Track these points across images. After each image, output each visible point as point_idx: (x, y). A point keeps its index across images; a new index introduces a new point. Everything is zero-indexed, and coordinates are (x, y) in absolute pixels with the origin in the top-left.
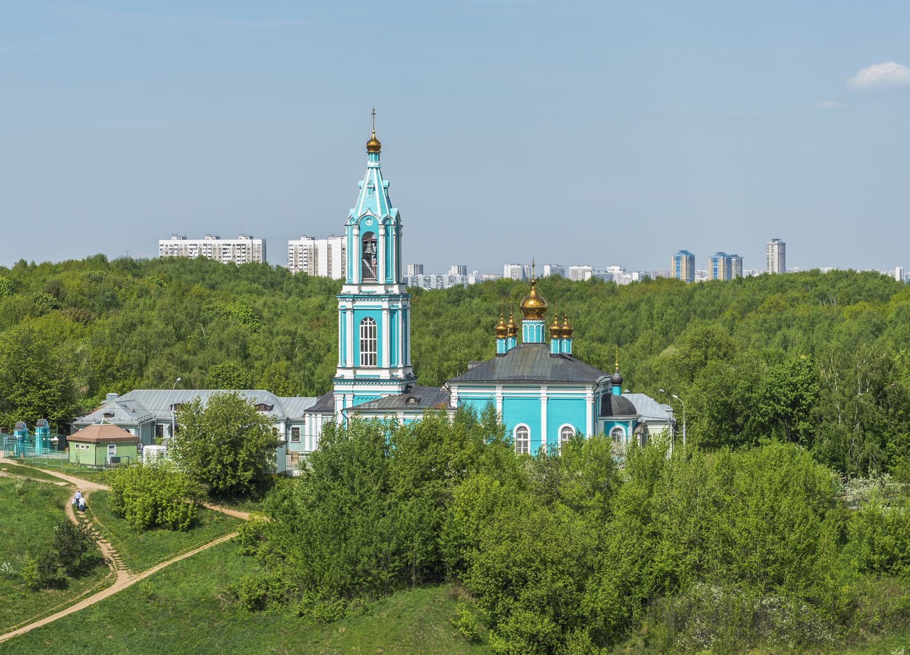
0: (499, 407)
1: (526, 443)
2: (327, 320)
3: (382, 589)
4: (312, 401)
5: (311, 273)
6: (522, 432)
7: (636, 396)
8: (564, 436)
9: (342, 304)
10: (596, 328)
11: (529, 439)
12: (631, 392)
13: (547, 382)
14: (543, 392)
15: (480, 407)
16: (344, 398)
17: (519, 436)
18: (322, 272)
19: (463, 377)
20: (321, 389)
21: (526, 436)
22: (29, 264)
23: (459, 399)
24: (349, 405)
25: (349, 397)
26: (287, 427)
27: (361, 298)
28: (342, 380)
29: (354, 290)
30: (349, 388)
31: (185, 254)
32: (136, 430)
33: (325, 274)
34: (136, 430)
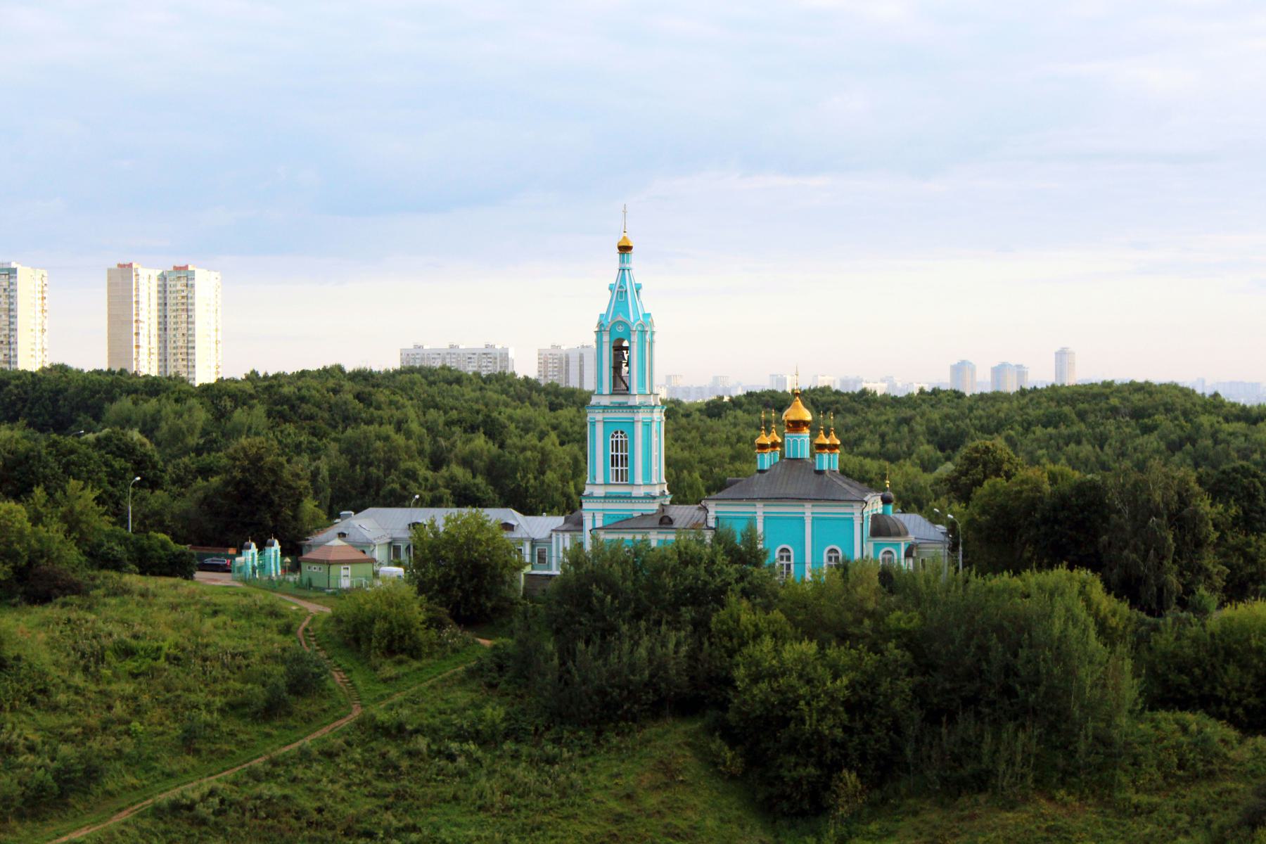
0: (760, 528)
1: (788, 566)
2: (577, 437)
3: (854, 479)
4: (559, 521)
5: (563, 385)
6: (785, 554)
7: (907, 516)
8: (830, 559)
9: (590, 417)
10: (872, 432)
11: (792, 561)
12: (903, 512)
13: (811, 500)
14: (808, 511)
15: (739, 528)
16: (593, 515)
17: (782, 558)
18: (574, 383)
19: (720, 495)
20: (569, 506)
21: (788, 558)
22: (261, 374)
23: (717, 518)
24: (599, 524)
25: (599, 517)
26: (533, 547)
27: (615, 362)
28: (590, 497)
29: (606, 401)
30: (600, 506)
31: (426, 364)
32: (370, 546)
33: (577, 386)
34: (370, 546)
